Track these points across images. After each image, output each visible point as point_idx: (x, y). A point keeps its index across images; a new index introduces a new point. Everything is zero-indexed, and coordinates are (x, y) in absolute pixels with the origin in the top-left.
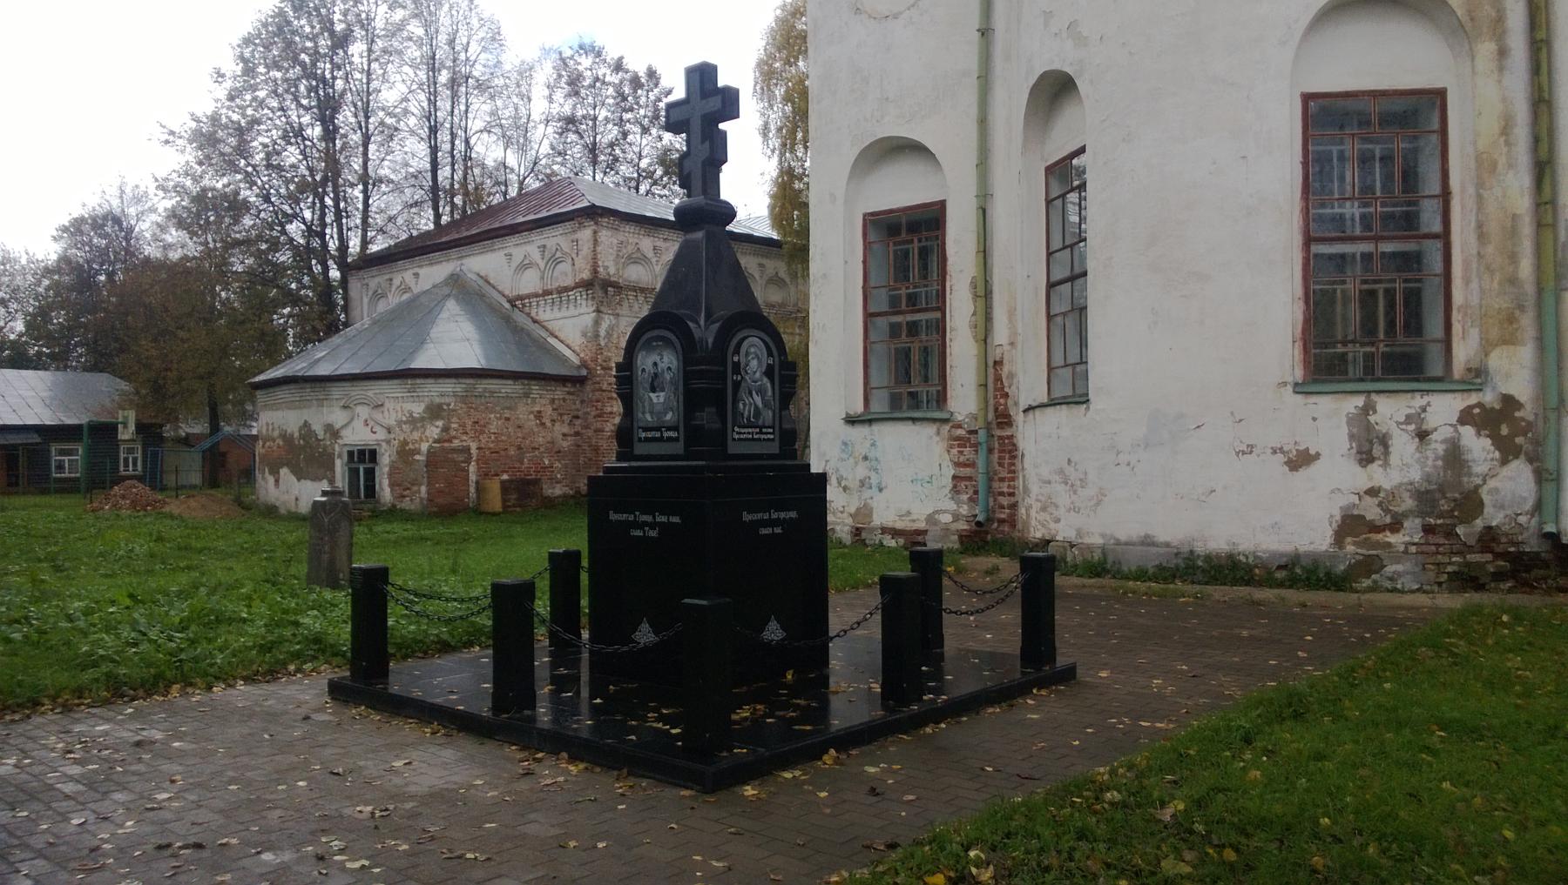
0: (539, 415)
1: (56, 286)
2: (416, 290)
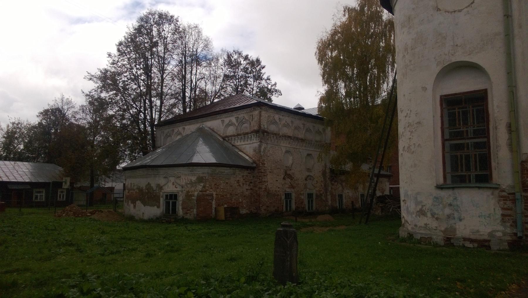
0: (238, 182)
1: (35, 133)
2: (184, 134)
